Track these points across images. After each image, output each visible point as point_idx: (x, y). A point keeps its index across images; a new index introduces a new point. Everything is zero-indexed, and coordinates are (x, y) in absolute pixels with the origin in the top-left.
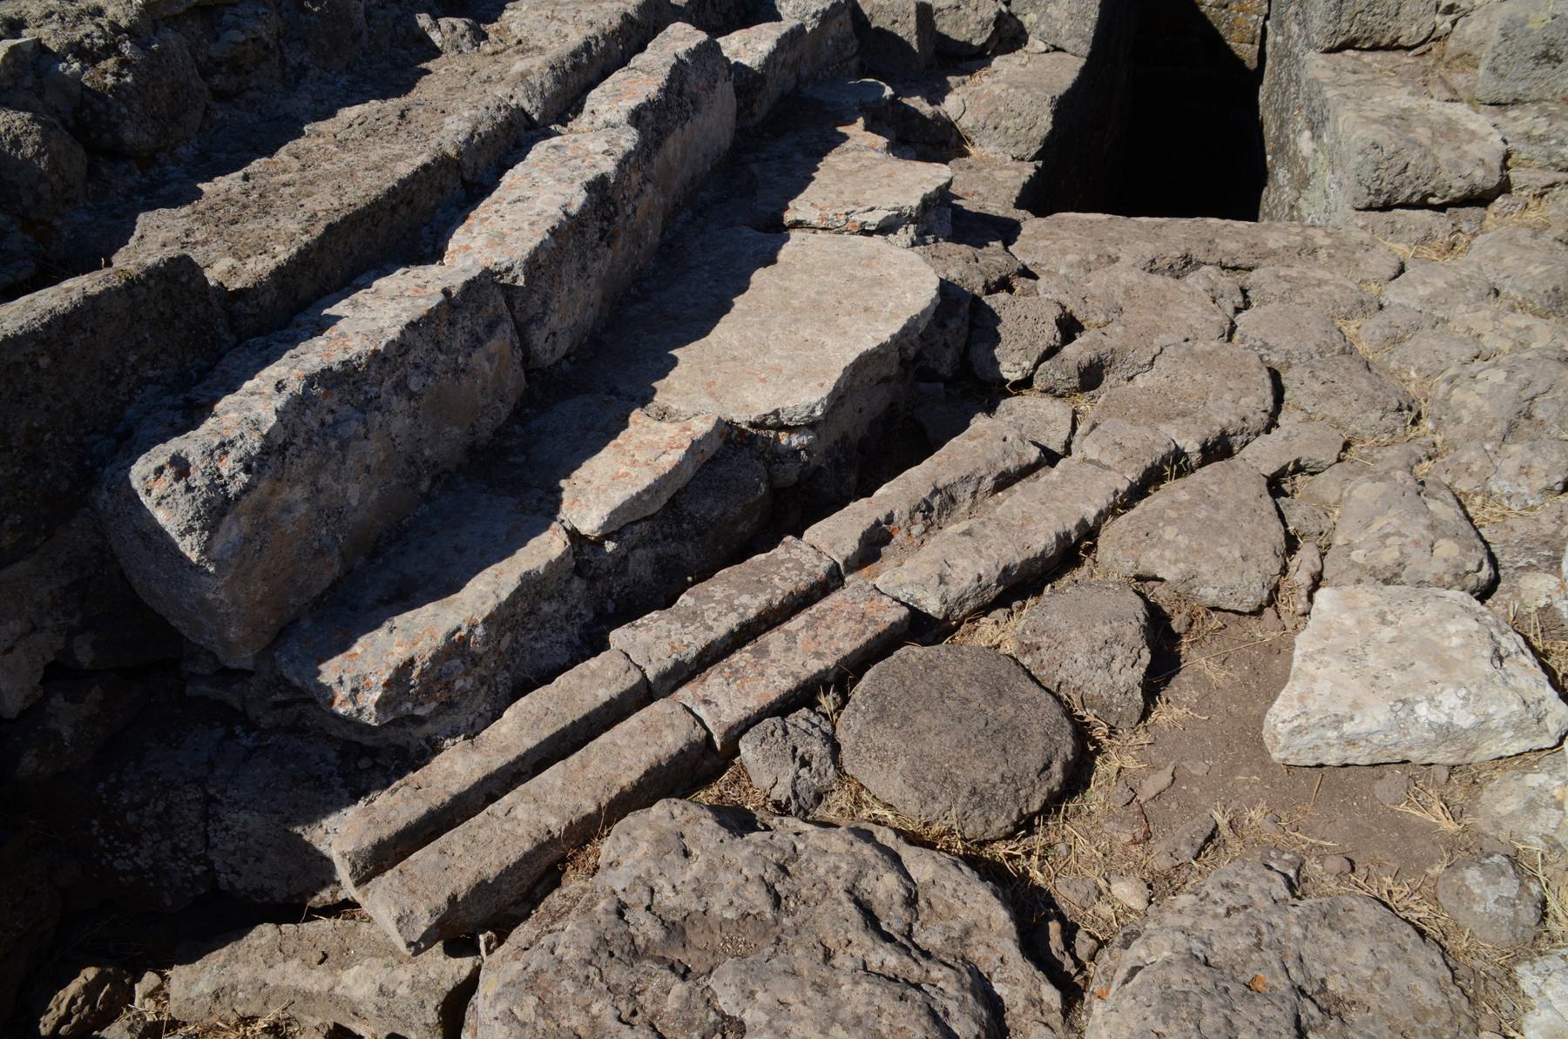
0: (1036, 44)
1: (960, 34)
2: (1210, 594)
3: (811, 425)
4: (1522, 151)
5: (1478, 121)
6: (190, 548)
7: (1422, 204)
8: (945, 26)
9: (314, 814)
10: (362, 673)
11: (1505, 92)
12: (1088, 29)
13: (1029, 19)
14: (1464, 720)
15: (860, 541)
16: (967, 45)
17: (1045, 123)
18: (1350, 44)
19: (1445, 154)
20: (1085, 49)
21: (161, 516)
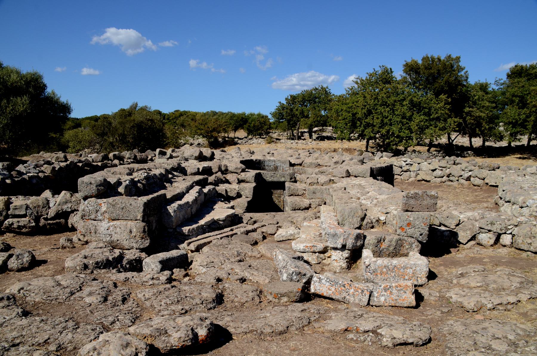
0: (243, 197)
1: (231, 195)
2: (269, 233)
3: (223, 221)
4: (312, 203)
5: (307, 200)
6: (172, 214)
7: (299, 210)
8: (229, 194)
9: (179, 244)
10: (186, 229)
11: (310, 198)
12: (252, 194)
13: (242, 193)
14: (293, 233)
15: (259, 115)
16: (233, 197)
17: (246, 205)
18: (292, 195)
19: (301, 203)
20: (251, 197)
21: (170, 211)
